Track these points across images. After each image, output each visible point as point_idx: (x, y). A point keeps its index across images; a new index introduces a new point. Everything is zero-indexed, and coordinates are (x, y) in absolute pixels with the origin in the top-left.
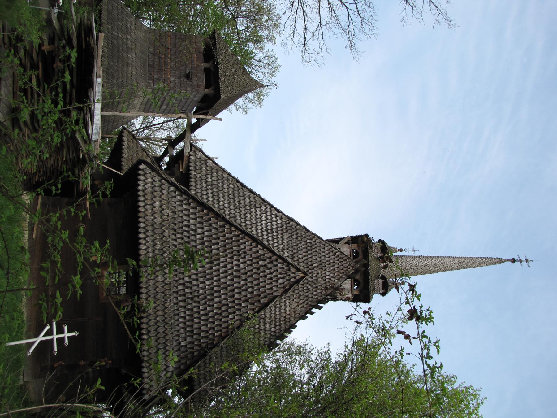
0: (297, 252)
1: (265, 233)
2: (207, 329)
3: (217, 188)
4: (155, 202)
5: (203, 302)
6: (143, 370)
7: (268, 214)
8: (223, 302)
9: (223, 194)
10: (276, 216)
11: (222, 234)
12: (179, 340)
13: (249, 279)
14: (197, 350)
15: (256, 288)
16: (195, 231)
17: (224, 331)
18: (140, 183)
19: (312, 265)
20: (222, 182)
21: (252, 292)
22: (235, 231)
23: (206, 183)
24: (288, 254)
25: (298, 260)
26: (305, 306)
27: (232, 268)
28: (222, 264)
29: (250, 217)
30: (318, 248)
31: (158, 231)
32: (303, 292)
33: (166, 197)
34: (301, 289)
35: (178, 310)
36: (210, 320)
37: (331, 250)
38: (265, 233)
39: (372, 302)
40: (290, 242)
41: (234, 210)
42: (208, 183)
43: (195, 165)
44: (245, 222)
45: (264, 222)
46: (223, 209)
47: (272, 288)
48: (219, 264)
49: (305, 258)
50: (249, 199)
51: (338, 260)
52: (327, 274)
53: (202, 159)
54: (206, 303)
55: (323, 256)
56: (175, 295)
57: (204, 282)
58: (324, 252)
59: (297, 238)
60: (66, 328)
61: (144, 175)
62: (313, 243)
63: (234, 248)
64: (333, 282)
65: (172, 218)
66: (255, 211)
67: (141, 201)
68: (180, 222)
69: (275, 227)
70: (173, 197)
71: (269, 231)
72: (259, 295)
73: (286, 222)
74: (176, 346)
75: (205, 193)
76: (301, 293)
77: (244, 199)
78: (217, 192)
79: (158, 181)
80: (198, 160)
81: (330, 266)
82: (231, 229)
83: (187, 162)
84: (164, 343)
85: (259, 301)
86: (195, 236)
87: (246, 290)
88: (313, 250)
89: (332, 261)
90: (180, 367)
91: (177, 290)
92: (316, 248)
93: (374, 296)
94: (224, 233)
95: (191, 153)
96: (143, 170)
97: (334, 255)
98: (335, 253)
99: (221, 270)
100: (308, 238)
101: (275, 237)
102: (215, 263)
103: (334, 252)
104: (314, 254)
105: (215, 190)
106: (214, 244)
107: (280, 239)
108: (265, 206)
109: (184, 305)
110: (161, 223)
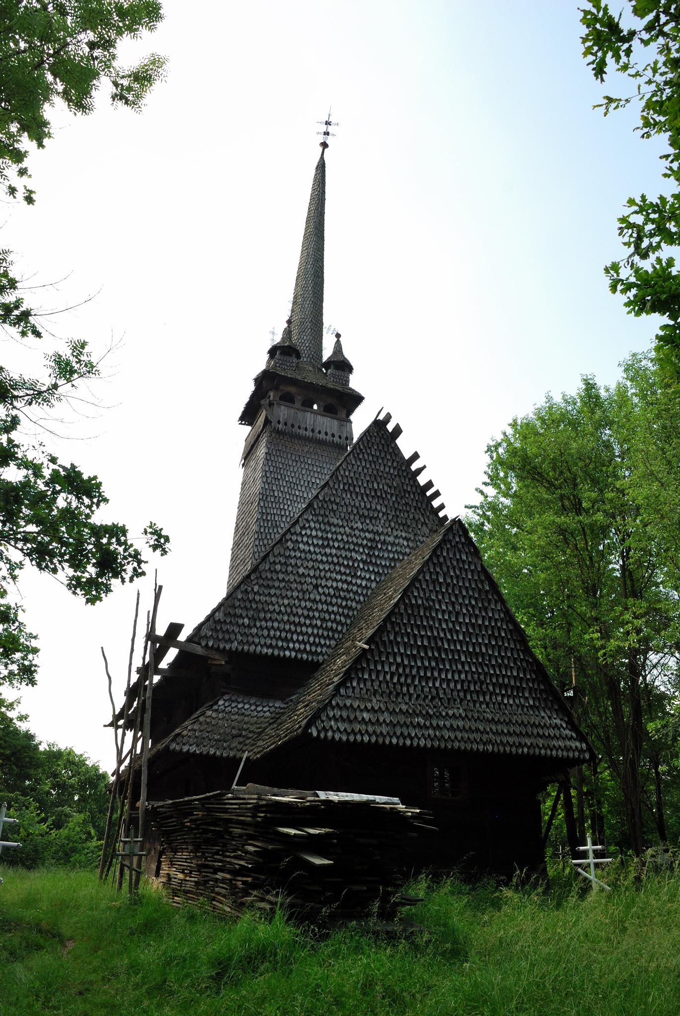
0: (357, 508)
1: (328, 551)
3: (259, 611)
4: (363, 719)
5: (486, 669)
6: (352, 740)
7: (300, 539)
9: (268, 604)
10: (303, 528)
11: (403, 628)
12: (527, 707)
13: (460, 600)
14: (538, 685)
16: (398, 665)
17: (518, 647)
20: (250, 602)
22: (399, 608)
23: (251, 628)
25: (368, 510)
26: (428, 514)
27: (446, 621)
29: (304, 568)
30: (352, 475)
34: (406, 514)
37: (356, 455)
38: (328, 551)
39: (363, 395)
41: (293, 591)
42: (252, 624)
44: (311, 578)
45: (312, 549)
46: (291, 608)
48: (441, 639)
49: (366, 499)
50: (276, 564)
52: (387, 470)
53: (213, 627)
54: (486, 665)
55: (363, 470)
56: (478, 705)
58: (358, 466)
60: (581, 848)
61: (326, 731)
62: (345, 481)
63: (422, 614)
69: (320, 534)
70: (353, 692)
71: (326, 543)
74: (534, 712)
75: (265, 632)
77: (277, 573)
79: (333, 710)
80: (215, 635)
82: (396, 613)
83: (214, 652)
85: (487, 592)
87: (473, 607)
89: (371, 458)
90: (556, 710)
92: (352, 478)
93: (353, 388)
94: (401, 624)
95: (203, 644)
96: (319, 732)
97: (363, 453)
98: (361, 450)
100: (336, 486)
102: (440, 644)
103: (358, 451)
106: (416, 642)
107: (338, 530)
108: (287, 541)
110: (391, 713)
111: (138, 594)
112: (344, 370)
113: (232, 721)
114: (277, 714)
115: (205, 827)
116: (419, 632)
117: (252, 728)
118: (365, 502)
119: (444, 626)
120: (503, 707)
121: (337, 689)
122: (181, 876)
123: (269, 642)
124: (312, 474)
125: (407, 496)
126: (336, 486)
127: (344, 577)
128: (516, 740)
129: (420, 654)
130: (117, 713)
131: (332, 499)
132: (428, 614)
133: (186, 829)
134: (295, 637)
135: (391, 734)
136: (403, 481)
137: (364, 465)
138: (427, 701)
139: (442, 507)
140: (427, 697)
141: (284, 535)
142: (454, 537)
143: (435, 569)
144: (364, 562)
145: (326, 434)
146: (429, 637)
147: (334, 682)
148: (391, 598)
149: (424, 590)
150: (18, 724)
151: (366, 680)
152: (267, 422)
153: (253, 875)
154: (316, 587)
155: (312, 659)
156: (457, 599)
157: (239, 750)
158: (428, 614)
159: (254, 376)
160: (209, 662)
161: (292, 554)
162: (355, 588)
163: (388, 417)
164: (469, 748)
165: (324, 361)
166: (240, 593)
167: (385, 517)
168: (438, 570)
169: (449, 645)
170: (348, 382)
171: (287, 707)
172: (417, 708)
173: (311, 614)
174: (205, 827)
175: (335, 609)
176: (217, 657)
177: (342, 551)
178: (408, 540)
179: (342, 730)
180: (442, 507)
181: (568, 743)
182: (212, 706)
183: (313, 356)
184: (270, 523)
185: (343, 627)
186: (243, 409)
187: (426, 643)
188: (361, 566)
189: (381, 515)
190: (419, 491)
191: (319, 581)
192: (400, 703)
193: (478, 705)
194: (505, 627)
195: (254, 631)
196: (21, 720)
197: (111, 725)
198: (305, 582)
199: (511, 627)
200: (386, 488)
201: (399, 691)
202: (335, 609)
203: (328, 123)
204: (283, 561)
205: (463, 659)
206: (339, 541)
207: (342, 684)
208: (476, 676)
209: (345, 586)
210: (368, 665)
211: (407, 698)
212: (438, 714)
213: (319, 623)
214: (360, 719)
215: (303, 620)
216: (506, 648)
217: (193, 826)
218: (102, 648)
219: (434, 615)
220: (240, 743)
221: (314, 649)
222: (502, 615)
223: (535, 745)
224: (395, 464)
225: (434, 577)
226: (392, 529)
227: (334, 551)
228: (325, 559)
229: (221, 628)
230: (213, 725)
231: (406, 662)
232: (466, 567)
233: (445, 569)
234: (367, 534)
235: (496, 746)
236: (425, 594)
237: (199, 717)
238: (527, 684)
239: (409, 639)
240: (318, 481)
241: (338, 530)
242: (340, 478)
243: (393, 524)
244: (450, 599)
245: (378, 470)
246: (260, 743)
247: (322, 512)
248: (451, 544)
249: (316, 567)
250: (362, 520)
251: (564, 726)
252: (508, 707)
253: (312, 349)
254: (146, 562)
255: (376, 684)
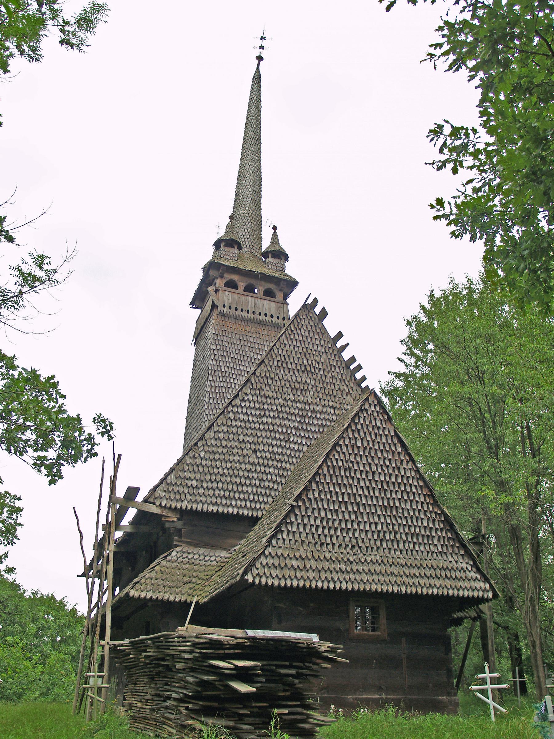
0: (289, 382)
1: (264, 420)
2: (426, 519)
5: (399, 520)
7: (240, 411)
8: (400, 497)
11: (326, 486)
12: (436, 553)
13: (376, 461)
14: (446, 533)
15: (385, 455)
16: (322, 519)
17: (428, 501)
18: (440, 593)
19: (305, 366)
20: (198, 466)
21: (390, 460)
22: (323, 469)
24: (291, 395)
26: (352, 385)
27: (364, 479)
28: (360, 492)
29: (244, 435)
30: (285, 353)
31: (326, 565)
32: (336, 384)
33: (286, 551)
34: (332, 386)
35: (407, 550)
36: (417, 514)
37: (288, 336)
38: (264, 420)
39: (298, 280)
40: (277, 388)
42: (199, 486)
43: (175, 500)
47: (386, 436)
48: (360, 495)
50: (220, 432)
51: (300, 329)
52: (315, 348)
53: (166, 489)
54: (400, 517)
55: (294, 348)
56: (392, 552)
57: (379, 516)
59: (272, 379)
63: (342, 474)
64: (326, 343)
65: (308, 545)
66: (235, 428)
67: (292, 583)
68: (313, 537)
69: (257, 405)
71: (262, 413)
72: (393, 452)
73: (251, 389)
75: (211, 492)
76: (337, 388)
78: (210, 474)
81: (306, 343)
83: (167, 510)
84: (440, 569)
85: (399, 453)
86: (328, 520)
88: (287, 360)
89: (301, 338)
90: (462, 555)
91: (387, 549)
92: (284, 356)
94: (325, 483)
95: (158, 504)
98: (292, 331)
99: (366, 493)
100: (271, 363)
101: (270, 407)
102: (358, 499)
103: (290, 332)
104: (292, 361)
105: (208, 477)
106: (337, 498)
107: (273, 401)
109: (402, 542)
111: (104, 460)
112: (280, 258)
113: (183, 569)
114: (222, 563)
115: (157, 662)
116: (340, 489)
117: (201, 575)
118: (296, 377)
119: (362, 484)
120: (414, 553)
121: (269, 541)
122: (139, 704)
123: (214, 500)
124: (254, 351)
125: (333, 370)
126: (271, 363)
127: (279, 443)
128: (427, 582)
129: (341, 509)
130: (88, 564)
131: (268, 375)
132: (348, 474)
133: (142, 664)
134: (237, 495)
135: (317, 578)
136: (329, 357)
137: (295, 344)
138: (348, 549)
139: (364, 379)
140: (348, 545)
141: (227, 407)
142: (370, 406)
143: (353, 434)
144: (296, 429)
145: (266, 315)
146: (349, 494)
147: (266, 535)
148: (316, 461)
149: (344, 453)
150: (6, 575)
151: (294, 532)
152: (214, 306)
153: (194, 701)
154: (255, 451)
155: (252, 514)
156: (373, 460)
157: (189, 595)
158: (348, 474)
159: (203, 266)
160: (163, 519)
161: (234, 423)
162: (288, 452)
163: (316, 301)
164: (385, 590)
165: (263, 251)
166: (188, 459)
167: (314, 389)
168: (356, 435)
169: (367, 501)
170: (284, 268)
171: (231, 557)
172: (339, 556)
173: (250, 475)
174: (157, 662)
175: (272, 470)
176: (169, 515)
177: (277, 420)
178: (334, 408)
179: (274, 576)
180: (364, 379)
181: (473, 584)
182: (166, 557)
183: (253, 246)
184: (218, 395)
185: (278, 486)
186: (193, 295)
187: (346, 499)
188: (294, 432)
189: (310, 387)
190: (344, 366)
191: (257, 447)
192: (324, 552)
193: (392, 552)
194: (415, 483)
195: (201, 491)
196: (8, 573)
197: (83, 575)
198: (245, 447)
199: (421, 483)
200: (314, 363)
201: (323, 541)
202: (272, 470)
203: (262, 38)
204: (225, 430)
205: (379, 512)
206: (274, 411)
207: (274, 536)
208: (390, 527)
209: (280, 450)
210: (296, 519)
211: (330, 547)
212: (357, 561)
213: (258, 483)
214: (290, 566)
215: (243, 480)
216: (417, 502)
217: (148, 661)
218: (74, 508)
219: (353, 474)
220: (190, 589)
221: (253, 505)
222: (413, 474)
223: (444, 586)
224: (322, 343)
225: (353, 442)
226: (320, 400)
227: (270, 420)
228: (262, 427)
229: (173, 489)
230: (167, 574)
231: (329, 516)
232: (381, 432)
233: (362, 435)
234: (298, 404)
235: (409, 587)
236: (345, 456)
237: (155, 566)
238: (436, 533)
239: (331, 496)
240: (259, 357)
241: (273, 401)
242: (274, 356)
243: (321, 395)
244: (367, 460)
245: (307, 348)
246: (207, 588)
247: (259, 387)
248: (367, 413)
249: (254, 435)
250: (294, 392)
251: (470, 568)
252: (420, 553)
253: (252, 240)
254: (98, 445)
255: (303, 535)
